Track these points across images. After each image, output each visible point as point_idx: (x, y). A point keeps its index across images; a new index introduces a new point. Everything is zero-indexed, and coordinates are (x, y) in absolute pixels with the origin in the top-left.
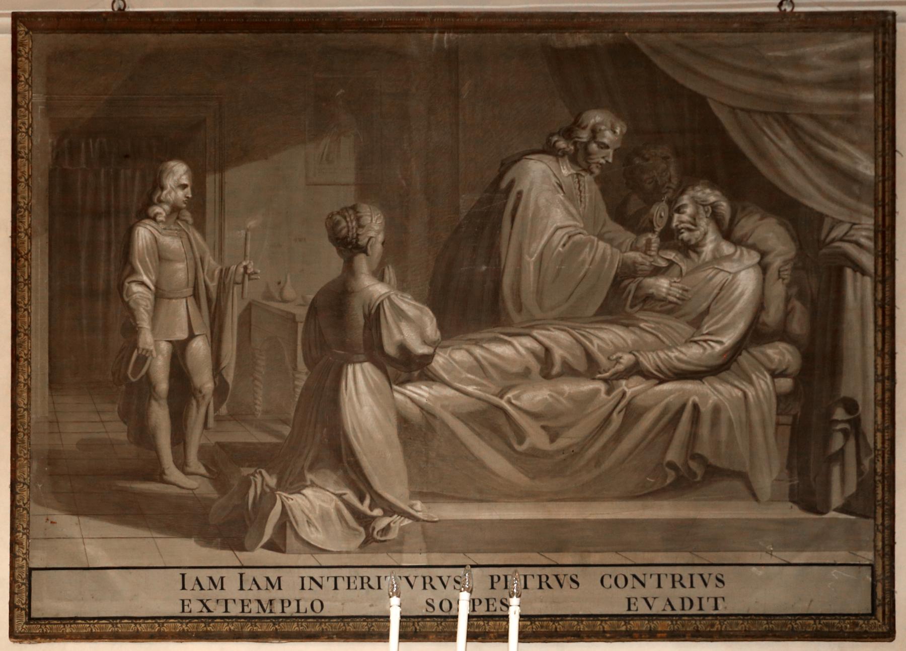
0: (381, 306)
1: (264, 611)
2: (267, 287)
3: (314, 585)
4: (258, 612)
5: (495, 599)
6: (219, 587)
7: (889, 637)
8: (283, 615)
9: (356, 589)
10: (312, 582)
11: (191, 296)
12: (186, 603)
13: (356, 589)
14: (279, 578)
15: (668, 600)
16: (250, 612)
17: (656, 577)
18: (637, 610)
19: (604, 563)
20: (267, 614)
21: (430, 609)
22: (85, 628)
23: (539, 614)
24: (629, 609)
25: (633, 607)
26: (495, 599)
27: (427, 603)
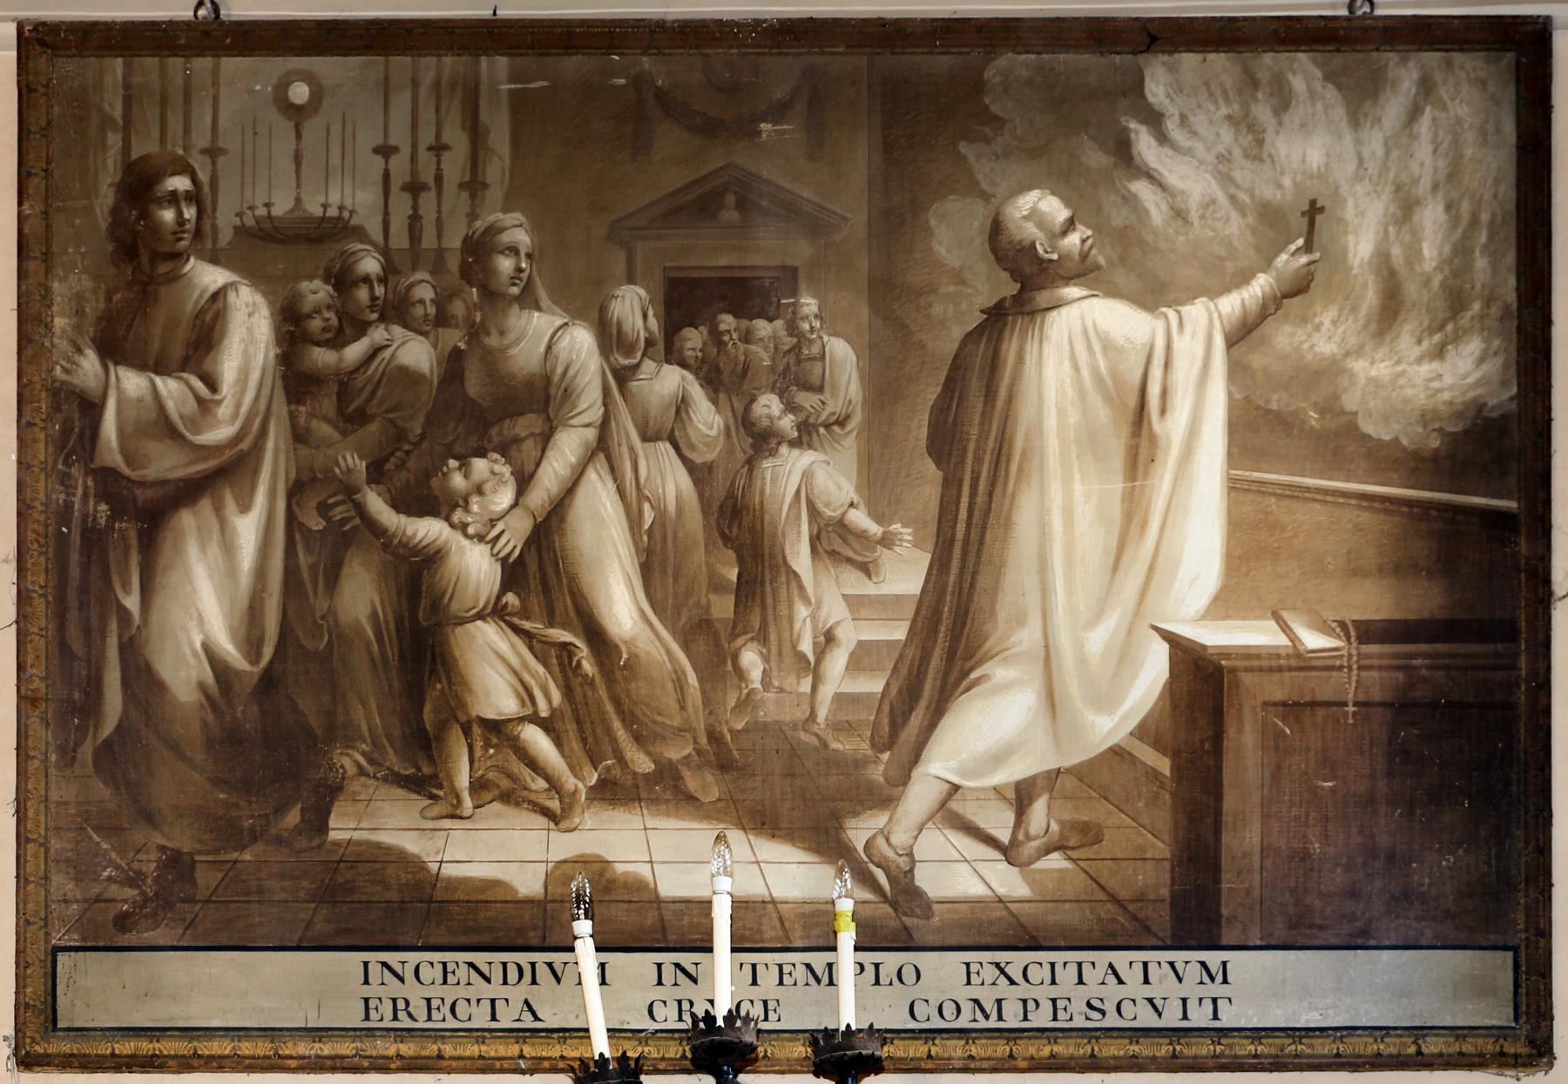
0: (221, 296)
1: (987, 1017)
2: (1280, 124)
3: (681, 977)
4: (975, 1020)
5: (443, 999)
6: (1219, 978)
7: (1541, 1055)
8: (1217, 1024)
9: (795, 984)
10: (678, 972)
11: (269, 212)
12: (372, 1004)
13: (795, 984)
14: (1224, 964)
15: (526, 1002)
16: (1071, 1019)
17: (1075, 967)
18: (1071, 1019)
19: (948, 943)
20: (993, 1023)
21: (1095, 1015)
22: (1325, 1047)
23: (59, 1017)
24: (367, 1018)
25: (1061, 1015)
26: (1134, 1001)
27: (1089, 1005)
